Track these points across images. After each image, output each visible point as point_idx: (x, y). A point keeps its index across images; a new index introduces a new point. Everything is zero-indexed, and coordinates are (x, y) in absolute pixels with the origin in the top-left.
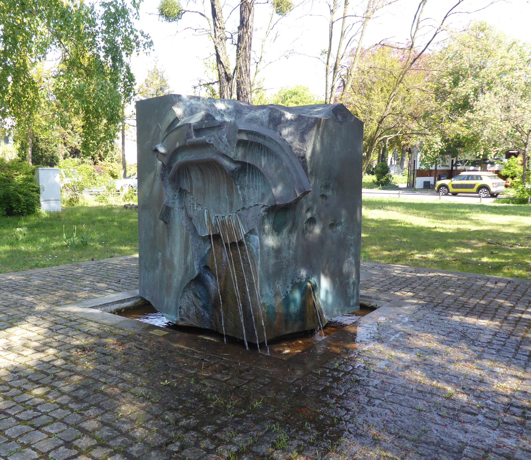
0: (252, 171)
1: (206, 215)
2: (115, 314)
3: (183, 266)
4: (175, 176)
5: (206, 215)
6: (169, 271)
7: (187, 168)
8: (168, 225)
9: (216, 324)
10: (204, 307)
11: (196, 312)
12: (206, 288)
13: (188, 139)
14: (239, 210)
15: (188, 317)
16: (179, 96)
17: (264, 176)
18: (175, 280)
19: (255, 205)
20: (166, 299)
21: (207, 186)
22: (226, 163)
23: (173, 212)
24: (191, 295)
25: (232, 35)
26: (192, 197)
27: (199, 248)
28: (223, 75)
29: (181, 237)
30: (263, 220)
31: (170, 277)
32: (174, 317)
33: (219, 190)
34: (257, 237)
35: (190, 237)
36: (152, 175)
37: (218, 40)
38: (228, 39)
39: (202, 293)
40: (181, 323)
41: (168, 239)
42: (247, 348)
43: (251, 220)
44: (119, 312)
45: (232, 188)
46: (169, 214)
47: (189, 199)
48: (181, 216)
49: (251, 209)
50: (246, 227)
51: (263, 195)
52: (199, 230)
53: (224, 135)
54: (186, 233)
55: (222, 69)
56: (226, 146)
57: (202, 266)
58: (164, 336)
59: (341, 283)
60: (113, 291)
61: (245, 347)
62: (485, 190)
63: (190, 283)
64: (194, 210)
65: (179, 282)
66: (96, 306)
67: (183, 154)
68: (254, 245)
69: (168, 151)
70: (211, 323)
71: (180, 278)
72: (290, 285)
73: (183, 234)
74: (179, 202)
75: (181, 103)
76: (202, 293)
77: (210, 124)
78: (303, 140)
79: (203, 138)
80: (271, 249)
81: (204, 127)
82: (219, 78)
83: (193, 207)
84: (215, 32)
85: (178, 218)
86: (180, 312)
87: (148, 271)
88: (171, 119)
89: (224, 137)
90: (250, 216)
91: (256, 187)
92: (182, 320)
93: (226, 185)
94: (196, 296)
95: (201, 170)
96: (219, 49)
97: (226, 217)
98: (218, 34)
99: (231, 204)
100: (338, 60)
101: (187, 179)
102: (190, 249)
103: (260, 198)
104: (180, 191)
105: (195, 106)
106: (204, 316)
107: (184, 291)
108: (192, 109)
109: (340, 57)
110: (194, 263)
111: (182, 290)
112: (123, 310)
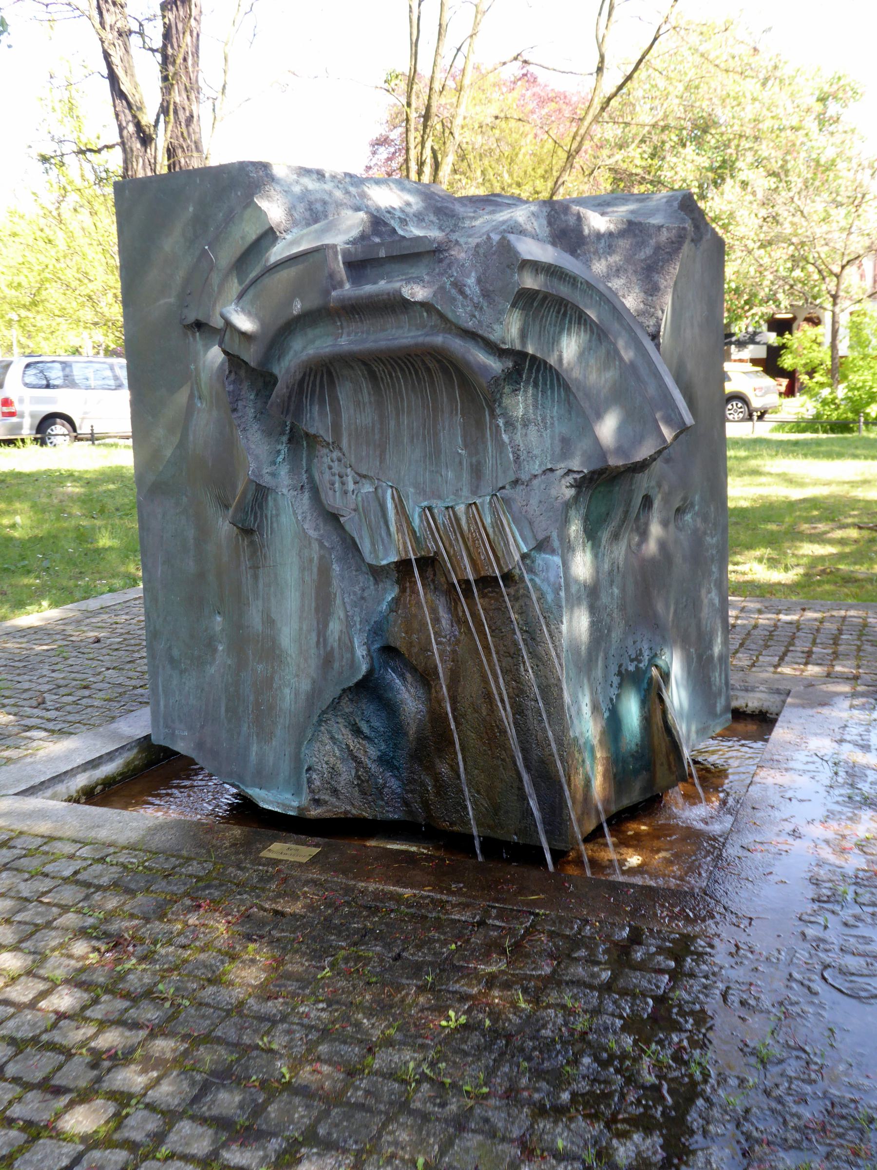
0: (537, 377)
1: (390, 505)
2: (77, 801)
3: (313, 651)
4: (290, 397)
5: (390, 505)
6: (260, 668)
7: (330, 374)
8: (256, 538)
9: (426, 804)
10: (384, 761)
11: (358, 777)
12: (389, 707)
13: (334, 289)
14: (503, 488)
15: (335, 792)
16: (265, 166)
17: (567, 388)
18: (287, 691)
19: (544, 472)
20: (254, 748)
21: (392, 423)
22: (481, 357)
23: (275, 500)
24: (345, 735)
25: (141, 25)
26: (336, 454)
27: (363, 598)
28: (131, 128)
29: (302, 569)
30: (567, 512)
31: (267, 683)
32: (289, 796)
33: (436, 434)
34: (557, 560)
35: (336, 567)
36: (182, 397)
37: (110, 36)
38: (133, 35)
39: (376, 724)
40: (315, 812)
41: (256, 577)
42: (480, 859)
43: (538, 513)
44: (90, 796)
45: (480, 425)
46: (261, 507)
47: (327, 460)
48: (299, 511)
49: (535, 482)
50: (527, 533)
51: (565, 442)
52: (366, 547)
53: (468, 276)
54: (321, 558)
55: (127, 111)
56: (477, 306)
57: (376, 646)
58: (314, 860)
59: (700, 657)
60: (43, 734)
61: (546, 865)
62: (740, 405)
63: (340, 698)
64: (346, 493)
65: (303, 697)
66: (32, 787)
67: (311, 333)
68: (546, 580)
69: (263, 324)
70: (406, 803)
71: (305, 686)
72: (616, 680)
73: (311, 560)
74: (292, 471)
75: (278, 188)
76: (376, 724)
77: (382, 249)
78: (652, 290)
79: (382, 286)
80: (582, 588)
81: (382, 254)
82: (121, 137)
83: (343, 484)
84: (101, 14)
85: (291, 518)
86: (310, 781)
87: (182, 672)
88: (252, 232)
89: (471, 281)
90: (534, 502)
91: (544, 419)
92: (317, 802)
93: (459, 418)
94: (357, 731)
95: (373, 377)
96: (116, 60)
97: (461, 509)
98: (109, 19)
99: (477, 471)
100: (435, 97)
101: (322, 402)
102: (338, 601)
103: (557, 450)
104: (290, 441)
105: (318, 196)
106: (384, 786)
107: (320, 722)
108: (310, 203)
109: (437, 86)
110: (352, 642)
111: (315, 719)
112: (99, 788)
